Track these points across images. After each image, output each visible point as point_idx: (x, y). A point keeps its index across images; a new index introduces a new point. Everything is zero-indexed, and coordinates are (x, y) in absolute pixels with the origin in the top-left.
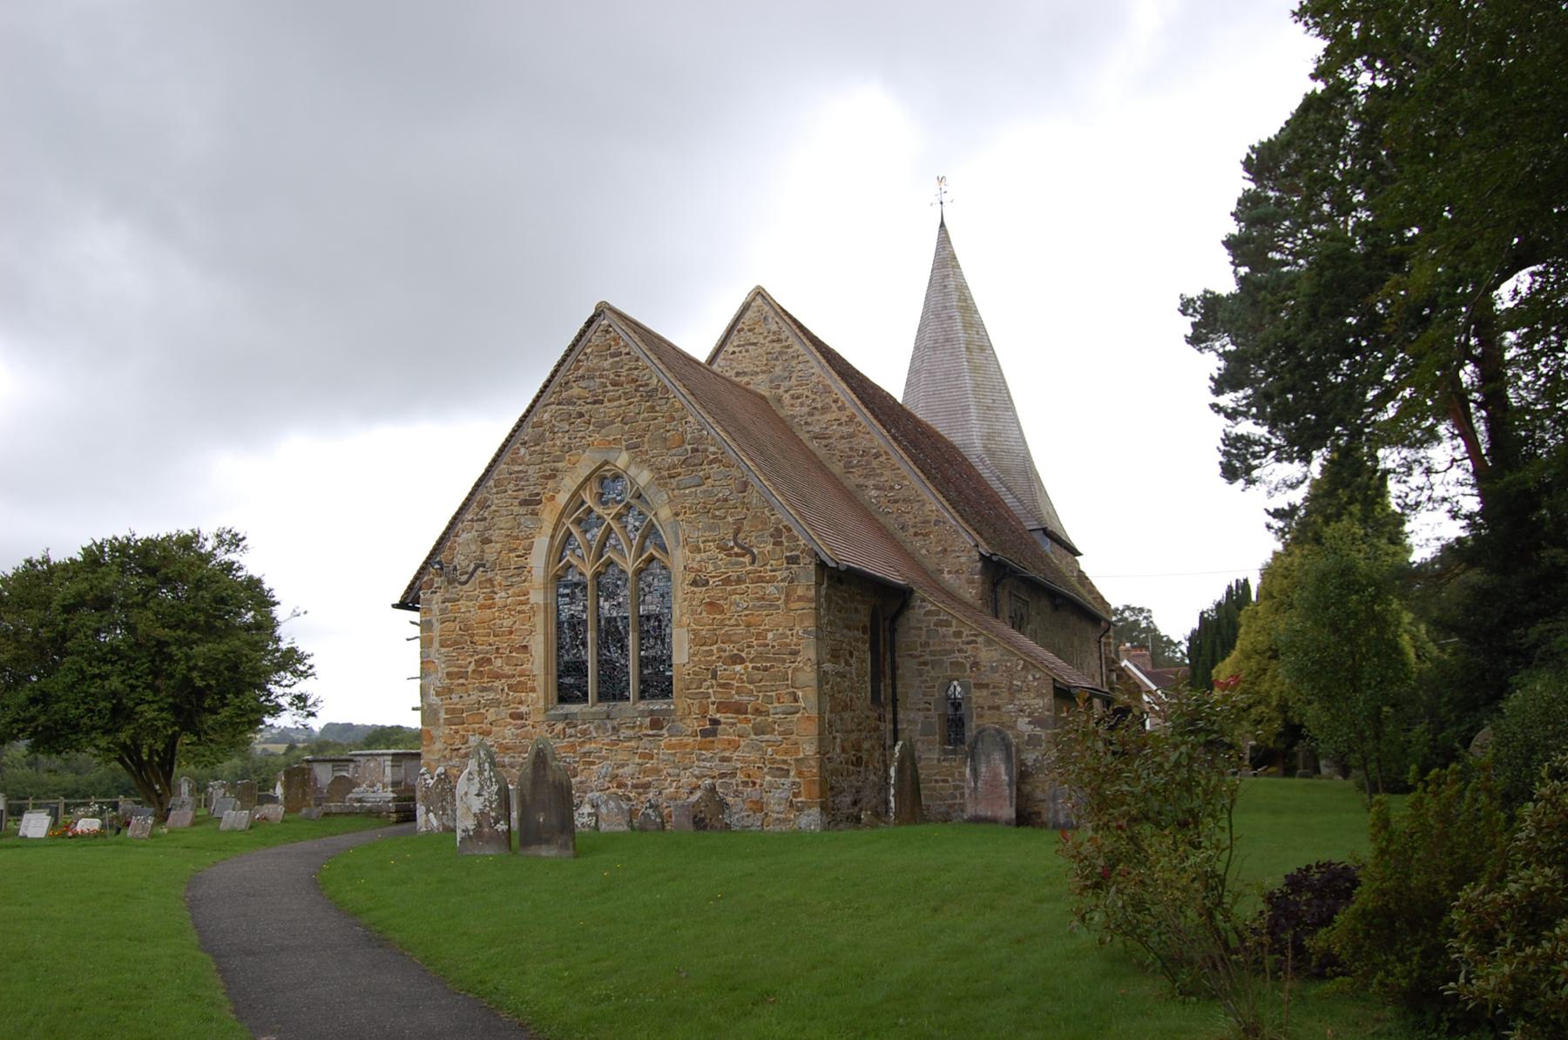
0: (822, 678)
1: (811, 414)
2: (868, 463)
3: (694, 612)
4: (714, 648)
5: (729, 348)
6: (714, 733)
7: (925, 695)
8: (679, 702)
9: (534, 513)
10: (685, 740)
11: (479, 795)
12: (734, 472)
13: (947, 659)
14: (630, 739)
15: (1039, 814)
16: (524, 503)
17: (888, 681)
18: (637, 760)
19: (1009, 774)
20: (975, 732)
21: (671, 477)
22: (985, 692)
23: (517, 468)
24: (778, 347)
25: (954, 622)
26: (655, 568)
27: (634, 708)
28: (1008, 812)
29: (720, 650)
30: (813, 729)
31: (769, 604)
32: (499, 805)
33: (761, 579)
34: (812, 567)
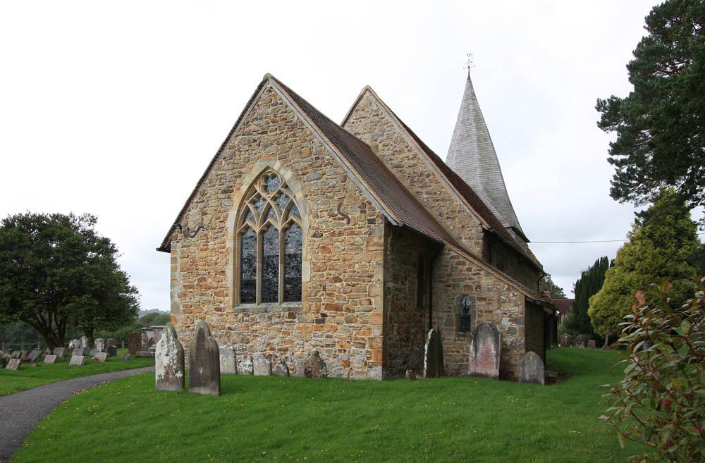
0: (386, 291)
1: (393, 154)
2: (423, 180)
3: (314, 252)
4: (325, 273)
5: (351, 120)
6: (323, 321)
7: (448, 303)
8: (304, 304)
10: (308, 325)
11: (167, 355)
12: (339, 170)
13: (462, 284)
14: (277, 323)
15: (512, 373)
16: (225, 192)
17: (428, 296)
18: (281, 335)
19: (496, 348)
20: (476, 326)
21: (303, 174)
22: (483, 303)
23: (220, 173)
24: (377, 119)
25: (467, 262)
26: (294, 228)
27: (279, 307)
28: (494, 371)
29: (328, 274)
30: (380, 320)
31: (356, 247)
32: (178, 362)
33: (353, 233)
34: (383, 225)
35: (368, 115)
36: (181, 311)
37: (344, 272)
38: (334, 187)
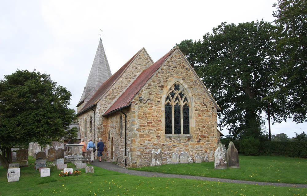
4: (200, 124)
9: (162, 89)
11: (220, 155)
14: (183, 142)
24: (147, 61)
33: (208, 111)
35: (143, 58)
36: (138, 137)
37: (206, 124)
38: (201, 94)
